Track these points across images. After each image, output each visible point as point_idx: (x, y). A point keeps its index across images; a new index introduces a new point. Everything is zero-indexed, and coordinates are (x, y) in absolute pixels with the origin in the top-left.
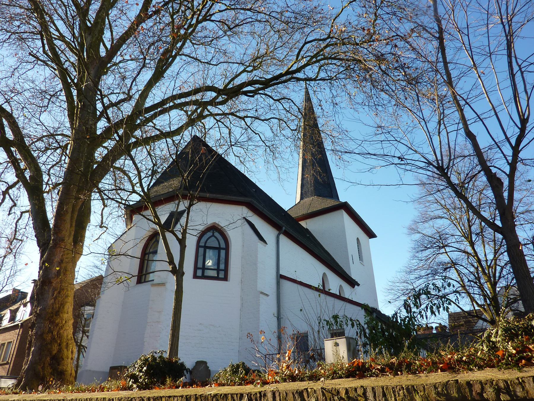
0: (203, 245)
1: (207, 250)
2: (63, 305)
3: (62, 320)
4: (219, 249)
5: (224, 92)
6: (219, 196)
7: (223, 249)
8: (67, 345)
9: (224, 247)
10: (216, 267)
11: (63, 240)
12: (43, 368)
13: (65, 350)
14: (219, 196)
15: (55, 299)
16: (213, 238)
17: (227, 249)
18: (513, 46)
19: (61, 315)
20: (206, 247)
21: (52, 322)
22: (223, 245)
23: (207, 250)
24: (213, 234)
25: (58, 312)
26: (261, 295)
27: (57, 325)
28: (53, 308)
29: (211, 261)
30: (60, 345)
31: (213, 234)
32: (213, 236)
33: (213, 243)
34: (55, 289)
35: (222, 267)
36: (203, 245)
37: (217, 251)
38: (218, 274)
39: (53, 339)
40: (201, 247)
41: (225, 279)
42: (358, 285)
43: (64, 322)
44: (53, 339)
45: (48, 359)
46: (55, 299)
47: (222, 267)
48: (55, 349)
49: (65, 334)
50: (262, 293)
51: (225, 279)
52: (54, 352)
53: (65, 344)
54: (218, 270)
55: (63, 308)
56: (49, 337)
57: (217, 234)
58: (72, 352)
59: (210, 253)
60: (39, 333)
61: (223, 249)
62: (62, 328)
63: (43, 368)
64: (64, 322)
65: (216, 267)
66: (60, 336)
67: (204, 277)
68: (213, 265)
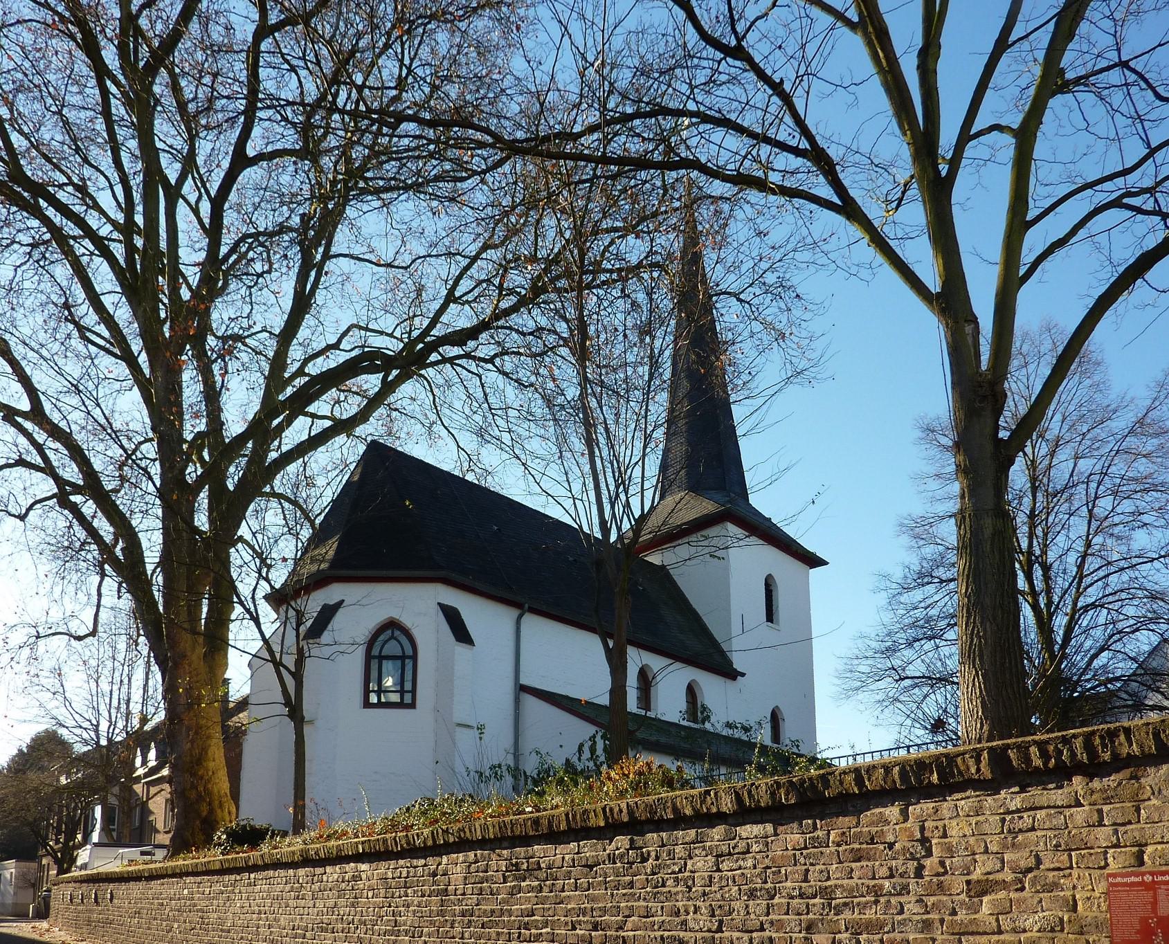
0: (377, 654)
1: (384, 662)
2: (205, 750)
3: (208, 770)
4: (403, 658)
5: (397, 363)
6: (384, 573)
7: (409, 657)
8: (221, 806)
9: (411, 654)
10: (398, 688)
11: (184, 656)
12: (193, 834)
13: (219, 811)
14: (384, 573)
15: (192, 742)
16: (393, 642)
17: (414, 658)
18: (297, 551)
19: (205, 764)
20: (381, 658)
21: (194, 775)
22: (409, 652)
23: (384, 662)
24: (393, 633)
25: (199, 759)
26: (459, 729)
27: (202, 778)
28: (191, 755)
29: (390, 679)
30: (210, 804)
31: (393, 633)
32: (393, 637)
33: (392, 648)
34: (189, 729)
35: (408, 686)
36: (377, 654)
37: (399, 663)
38: (402, 698)
39: (200, 798)
40: (375, 657)
41: (412, 706)
42: (743, 675)
43: (210, 773)
44: (200, 798)
45: (198, 822)
46: (192, 742)
47: (408, 686)
48: (204, 811)
49: (216, 790)
50: (459, 725)
51: (412, 706)
52: (204, 814)
53: (217, 803)
54: (402, 692)
55: (206, 753)
56: (193, 795)
57: (397, 633)
58: (229, 813)
59: (388, 665)
60: (179, 789)
61: (409, 657)
62: (209, 781)
63: (193, 834)
64: (210, 773)
65: (398, 688)
66: (209, 793)
67: (380, 705)
68: (395, 684)
